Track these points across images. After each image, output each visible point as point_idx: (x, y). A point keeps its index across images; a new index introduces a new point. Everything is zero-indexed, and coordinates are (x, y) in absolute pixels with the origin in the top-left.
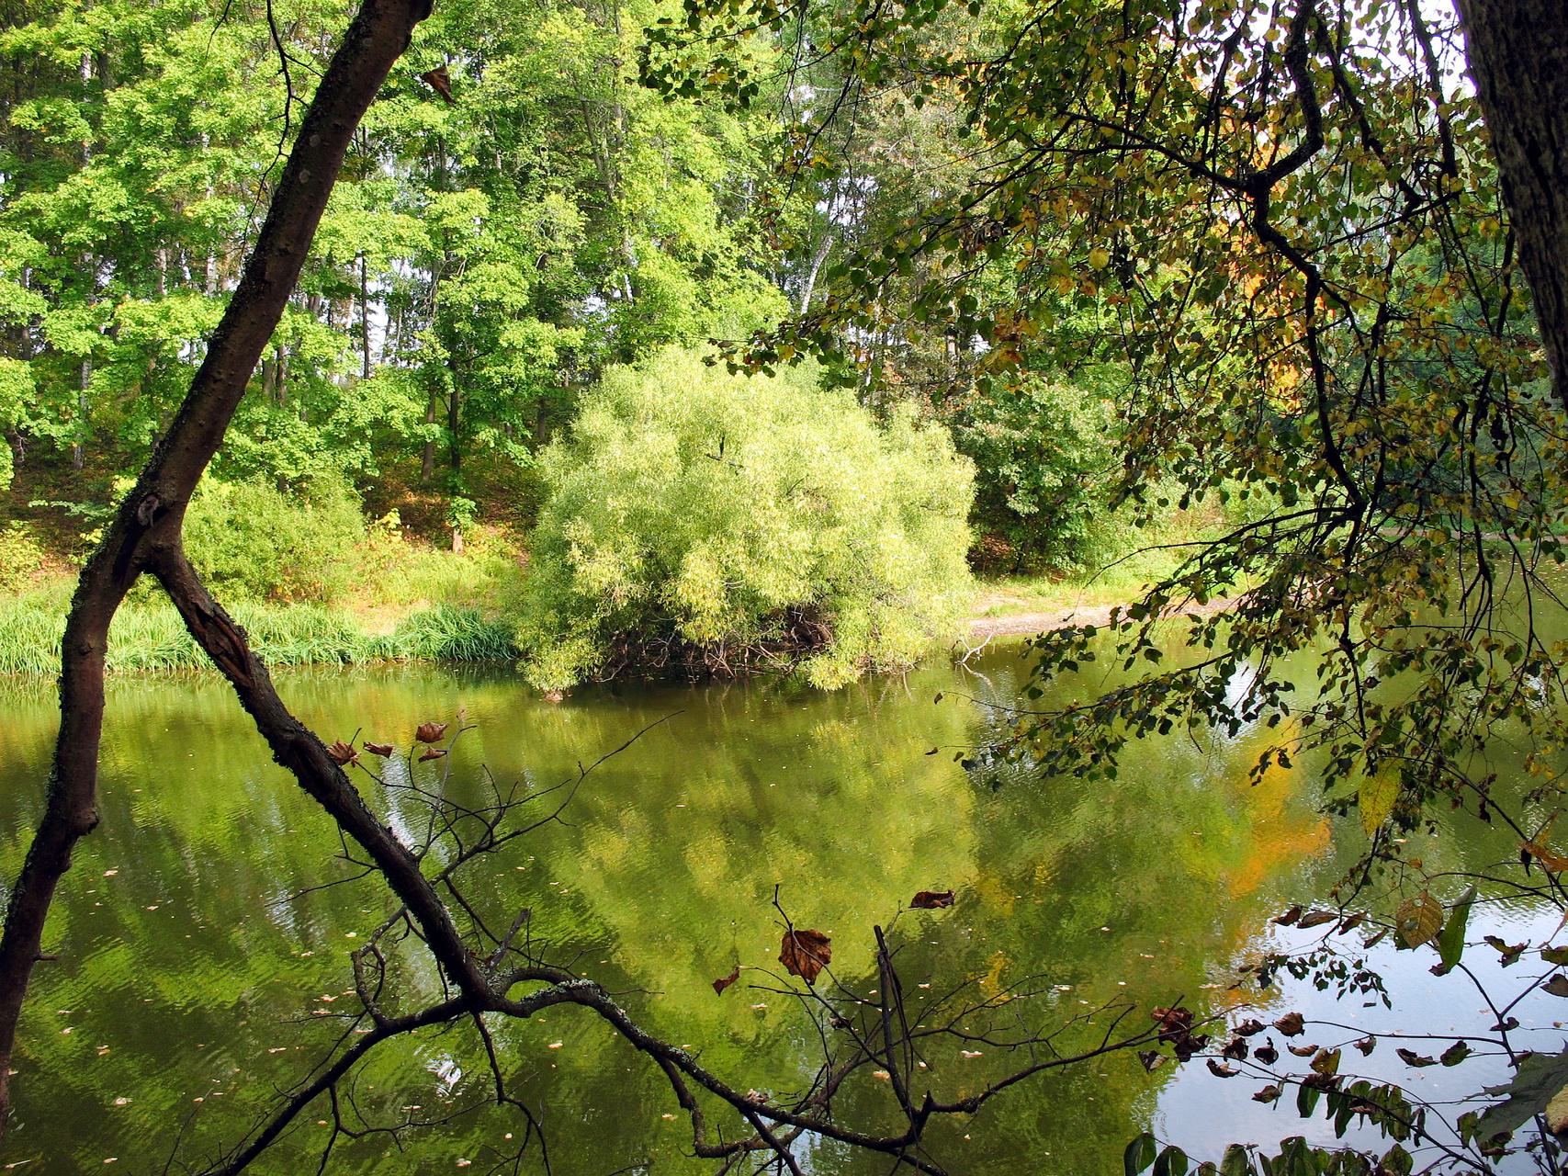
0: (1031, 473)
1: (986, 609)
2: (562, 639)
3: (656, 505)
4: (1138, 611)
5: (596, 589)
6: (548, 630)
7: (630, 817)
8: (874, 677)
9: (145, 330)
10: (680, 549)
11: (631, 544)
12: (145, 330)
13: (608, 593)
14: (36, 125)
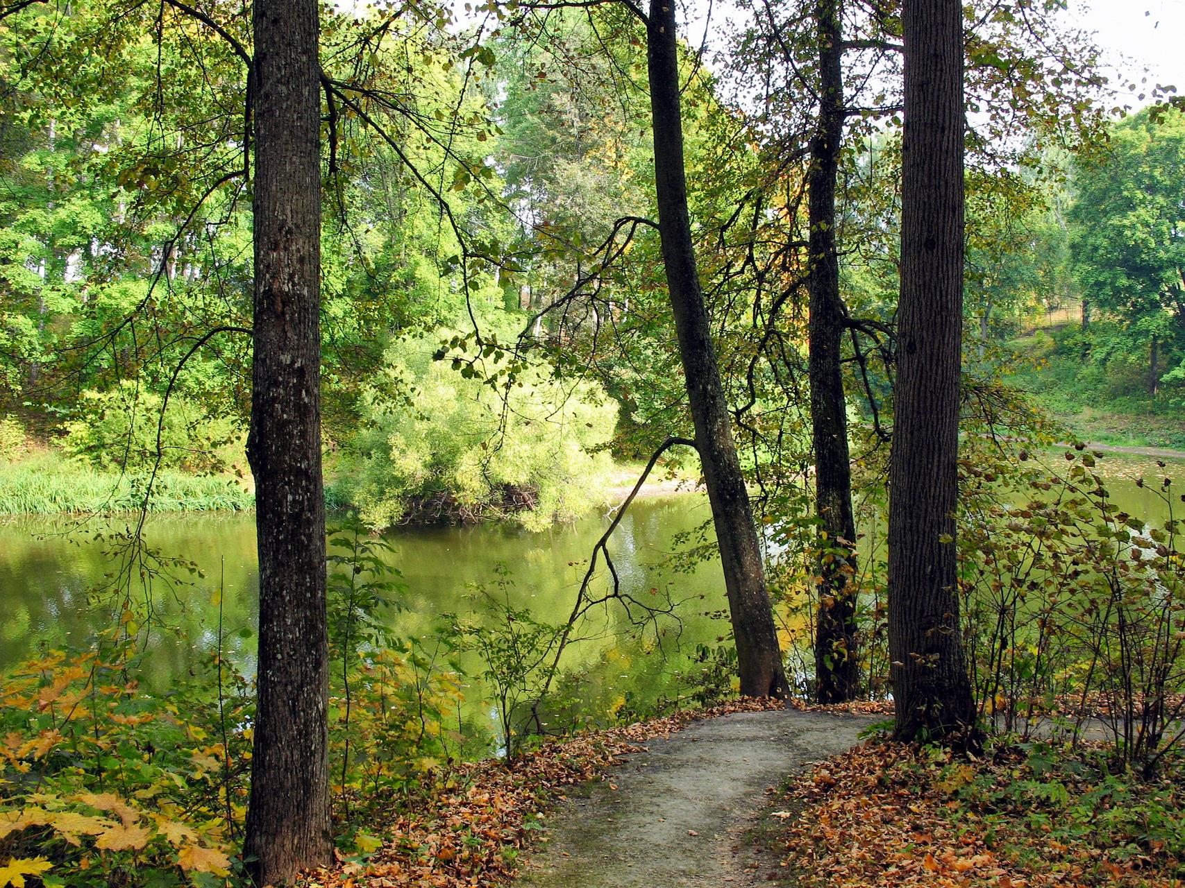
0: (648, 400)
1: (618, 481)
2: (381, 500)
3: (441, 427)
4: (701, 528)
5: (406, 472)
6: (372, 495)
7: (421, 602)
8: (558, 524)
9: (113, 302)
10: (455, 452)
11: (426, 448)
12: (113, 302)
13: (413, 475)
14: (39, 168)
